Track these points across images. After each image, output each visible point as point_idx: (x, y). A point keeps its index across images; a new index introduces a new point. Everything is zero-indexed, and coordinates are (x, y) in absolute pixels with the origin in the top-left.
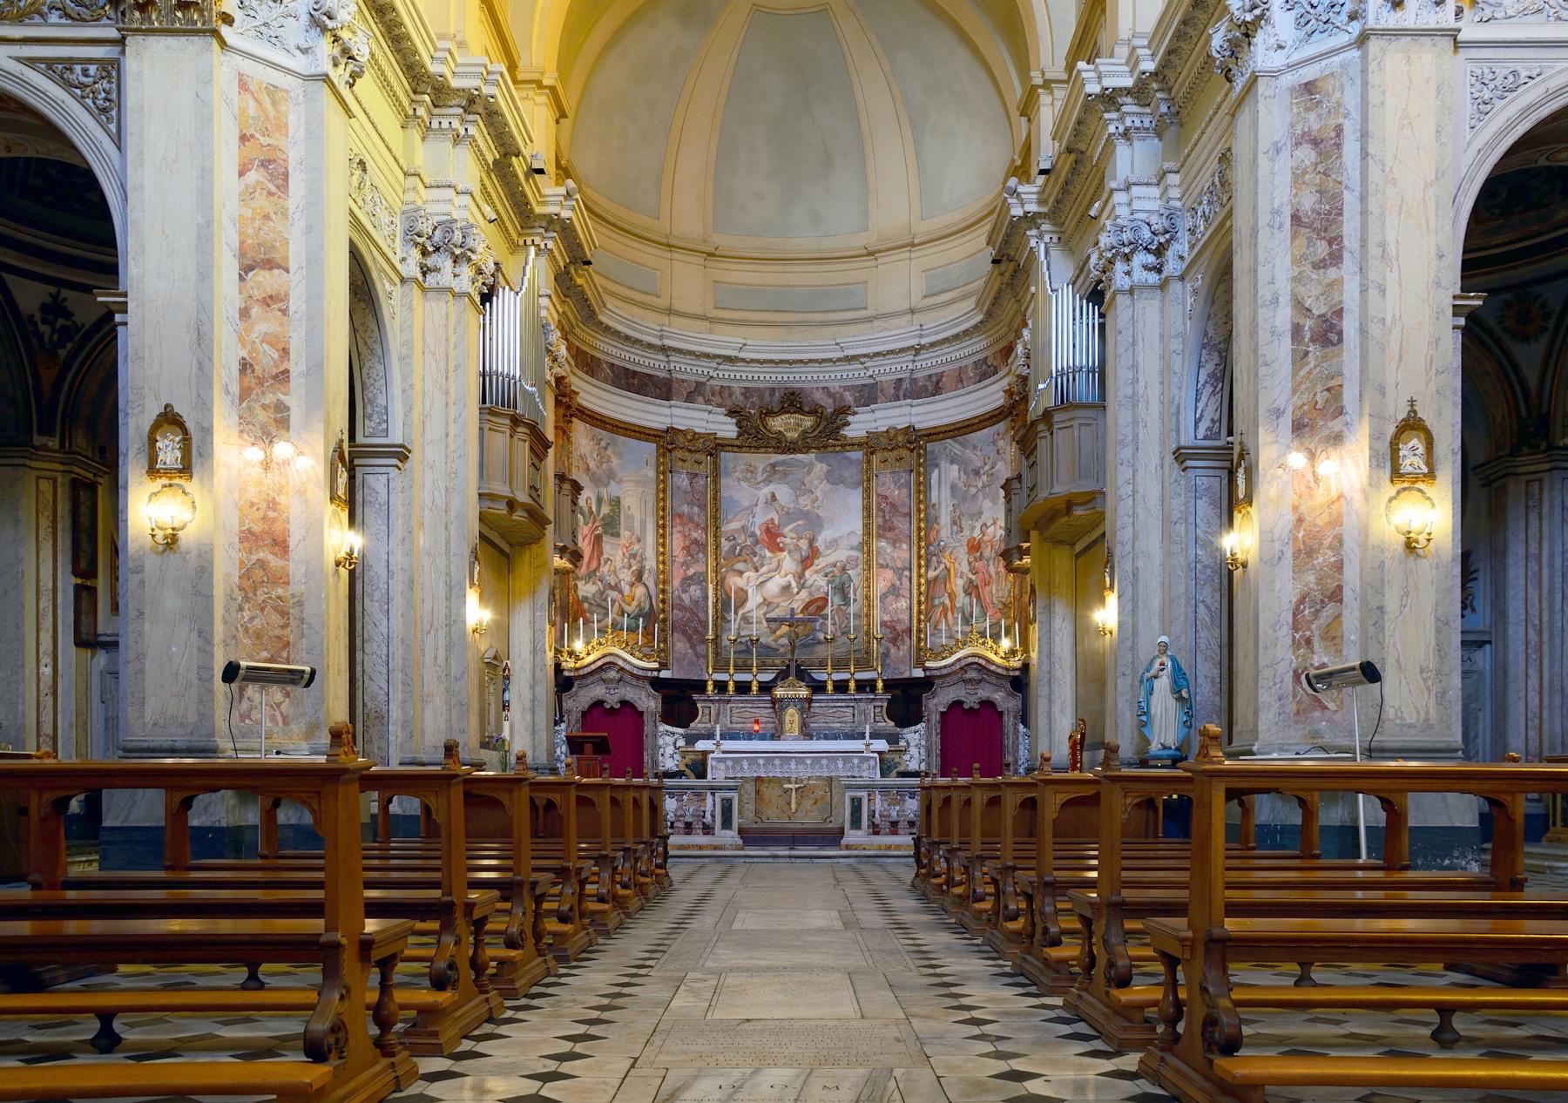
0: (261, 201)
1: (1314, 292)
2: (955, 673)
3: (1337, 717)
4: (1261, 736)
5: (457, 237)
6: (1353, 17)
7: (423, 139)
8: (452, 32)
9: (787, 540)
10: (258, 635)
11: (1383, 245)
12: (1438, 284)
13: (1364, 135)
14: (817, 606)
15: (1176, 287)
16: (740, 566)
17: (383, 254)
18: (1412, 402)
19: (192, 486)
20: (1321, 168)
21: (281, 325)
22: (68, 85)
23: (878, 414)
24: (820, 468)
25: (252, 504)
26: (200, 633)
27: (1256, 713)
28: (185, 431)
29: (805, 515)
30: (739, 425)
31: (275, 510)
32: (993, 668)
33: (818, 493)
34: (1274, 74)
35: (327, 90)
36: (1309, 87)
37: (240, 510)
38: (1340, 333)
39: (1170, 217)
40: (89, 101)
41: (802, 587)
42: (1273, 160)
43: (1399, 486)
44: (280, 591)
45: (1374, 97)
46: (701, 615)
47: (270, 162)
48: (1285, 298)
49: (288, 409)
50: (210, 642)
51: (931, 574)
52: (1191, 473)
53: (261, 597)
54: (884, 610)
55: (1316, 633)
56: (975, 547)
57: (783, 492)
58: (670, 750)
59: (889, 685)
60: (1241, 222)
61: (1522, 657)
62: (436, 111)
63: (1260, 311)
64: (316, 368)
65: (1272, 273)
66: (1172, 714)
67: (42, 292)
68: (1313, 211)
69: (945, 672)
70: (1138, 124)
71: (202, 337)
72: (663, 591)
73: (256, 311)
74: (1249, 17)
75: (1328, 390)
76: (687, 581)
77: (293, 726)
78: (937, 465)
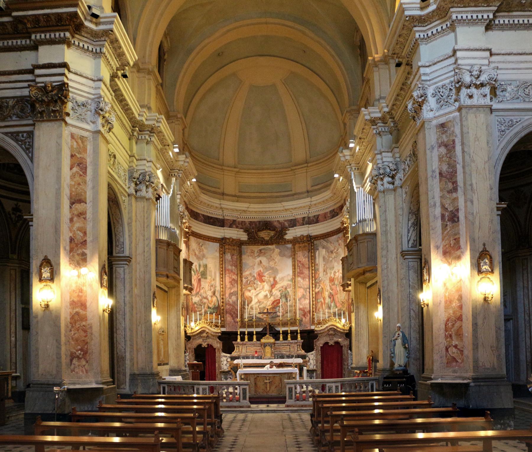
0: (77, 178)
1: (448, 202)
2: (326, 332)
3: (462, 365)
4: (435, 372)
5: (147, 178)
6: (456, 101)
7: (136, 143)
8: (146, 103)
9: (266, 278)
10: (77, 340)
11: (471, 185)
12: (491, 199)
13: (463, 144)
14: (276, 304)
15: (399, 190)
16: (249, 288)
17: (122, 187)
18: (484, 245)
19: (53, 285)
20: (448, 155)
21: (84, 223)
22: (17, 141)
23: (297, 230)
24: (277, 250)
25: (74, 291)
26: (56, 341)
27: (433, 363)
28: (51, 266)
29: (272, 268)
30: (248, 235)
31: (82, 292)
32: (339, 330)
33: (276, 260)
34: (430, 121)
35: (100, 136)
36: (443, 125)
37: (70, 293)
38: (458, 218)
39: (396, 164)
40: (23, 146)
41: (271, 295)
42: (431, 152)
43: (481, 276)
44: (84, 323)
45: (465, 130)
46: (236, 307)
47: (81, 164)
48: (438, 204)
49: (86, 255)
50: (60, 344)
51: (317, 290)
52: (407, 261)
53: (78, 326)
54: (300, 304)
55: (454, 332)
56: (332, 280)
57: (264, 259)
58: (225, 362)
59: (302, 332)
60: (421, 173)
61: (523, 325)
62: (140, 133)
63: (430, 209)
64: (96, 239)
65: (433, 191)
66: (402, 353)
67: (12, 203)
68: (447, 171)
69: (322, 332)
70: (383, 130)
71: (57, 231)
72: (223, 299)
73: (75, 219)
74: (420, 100)
75: (455, 239)
76: (231, 294)
77: (89, 374)
78: (318, 249)
